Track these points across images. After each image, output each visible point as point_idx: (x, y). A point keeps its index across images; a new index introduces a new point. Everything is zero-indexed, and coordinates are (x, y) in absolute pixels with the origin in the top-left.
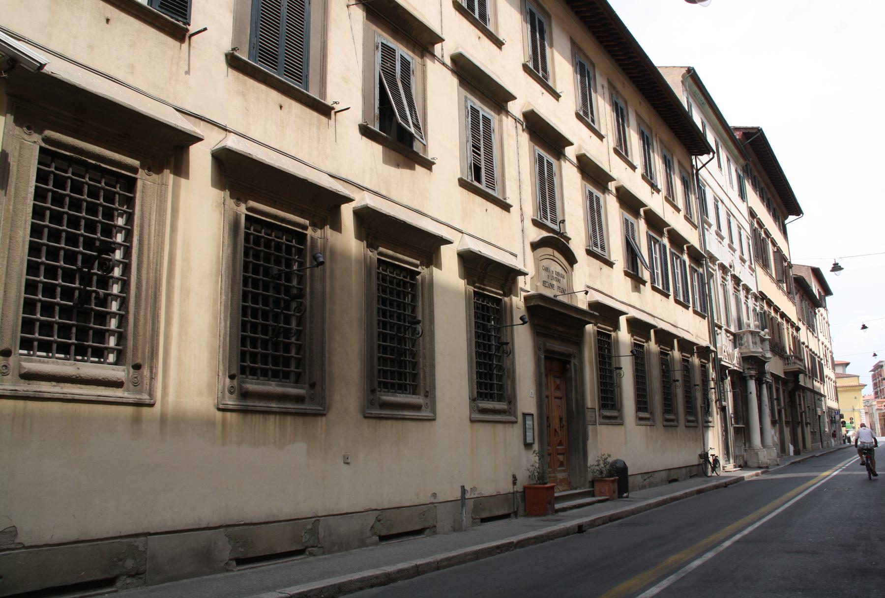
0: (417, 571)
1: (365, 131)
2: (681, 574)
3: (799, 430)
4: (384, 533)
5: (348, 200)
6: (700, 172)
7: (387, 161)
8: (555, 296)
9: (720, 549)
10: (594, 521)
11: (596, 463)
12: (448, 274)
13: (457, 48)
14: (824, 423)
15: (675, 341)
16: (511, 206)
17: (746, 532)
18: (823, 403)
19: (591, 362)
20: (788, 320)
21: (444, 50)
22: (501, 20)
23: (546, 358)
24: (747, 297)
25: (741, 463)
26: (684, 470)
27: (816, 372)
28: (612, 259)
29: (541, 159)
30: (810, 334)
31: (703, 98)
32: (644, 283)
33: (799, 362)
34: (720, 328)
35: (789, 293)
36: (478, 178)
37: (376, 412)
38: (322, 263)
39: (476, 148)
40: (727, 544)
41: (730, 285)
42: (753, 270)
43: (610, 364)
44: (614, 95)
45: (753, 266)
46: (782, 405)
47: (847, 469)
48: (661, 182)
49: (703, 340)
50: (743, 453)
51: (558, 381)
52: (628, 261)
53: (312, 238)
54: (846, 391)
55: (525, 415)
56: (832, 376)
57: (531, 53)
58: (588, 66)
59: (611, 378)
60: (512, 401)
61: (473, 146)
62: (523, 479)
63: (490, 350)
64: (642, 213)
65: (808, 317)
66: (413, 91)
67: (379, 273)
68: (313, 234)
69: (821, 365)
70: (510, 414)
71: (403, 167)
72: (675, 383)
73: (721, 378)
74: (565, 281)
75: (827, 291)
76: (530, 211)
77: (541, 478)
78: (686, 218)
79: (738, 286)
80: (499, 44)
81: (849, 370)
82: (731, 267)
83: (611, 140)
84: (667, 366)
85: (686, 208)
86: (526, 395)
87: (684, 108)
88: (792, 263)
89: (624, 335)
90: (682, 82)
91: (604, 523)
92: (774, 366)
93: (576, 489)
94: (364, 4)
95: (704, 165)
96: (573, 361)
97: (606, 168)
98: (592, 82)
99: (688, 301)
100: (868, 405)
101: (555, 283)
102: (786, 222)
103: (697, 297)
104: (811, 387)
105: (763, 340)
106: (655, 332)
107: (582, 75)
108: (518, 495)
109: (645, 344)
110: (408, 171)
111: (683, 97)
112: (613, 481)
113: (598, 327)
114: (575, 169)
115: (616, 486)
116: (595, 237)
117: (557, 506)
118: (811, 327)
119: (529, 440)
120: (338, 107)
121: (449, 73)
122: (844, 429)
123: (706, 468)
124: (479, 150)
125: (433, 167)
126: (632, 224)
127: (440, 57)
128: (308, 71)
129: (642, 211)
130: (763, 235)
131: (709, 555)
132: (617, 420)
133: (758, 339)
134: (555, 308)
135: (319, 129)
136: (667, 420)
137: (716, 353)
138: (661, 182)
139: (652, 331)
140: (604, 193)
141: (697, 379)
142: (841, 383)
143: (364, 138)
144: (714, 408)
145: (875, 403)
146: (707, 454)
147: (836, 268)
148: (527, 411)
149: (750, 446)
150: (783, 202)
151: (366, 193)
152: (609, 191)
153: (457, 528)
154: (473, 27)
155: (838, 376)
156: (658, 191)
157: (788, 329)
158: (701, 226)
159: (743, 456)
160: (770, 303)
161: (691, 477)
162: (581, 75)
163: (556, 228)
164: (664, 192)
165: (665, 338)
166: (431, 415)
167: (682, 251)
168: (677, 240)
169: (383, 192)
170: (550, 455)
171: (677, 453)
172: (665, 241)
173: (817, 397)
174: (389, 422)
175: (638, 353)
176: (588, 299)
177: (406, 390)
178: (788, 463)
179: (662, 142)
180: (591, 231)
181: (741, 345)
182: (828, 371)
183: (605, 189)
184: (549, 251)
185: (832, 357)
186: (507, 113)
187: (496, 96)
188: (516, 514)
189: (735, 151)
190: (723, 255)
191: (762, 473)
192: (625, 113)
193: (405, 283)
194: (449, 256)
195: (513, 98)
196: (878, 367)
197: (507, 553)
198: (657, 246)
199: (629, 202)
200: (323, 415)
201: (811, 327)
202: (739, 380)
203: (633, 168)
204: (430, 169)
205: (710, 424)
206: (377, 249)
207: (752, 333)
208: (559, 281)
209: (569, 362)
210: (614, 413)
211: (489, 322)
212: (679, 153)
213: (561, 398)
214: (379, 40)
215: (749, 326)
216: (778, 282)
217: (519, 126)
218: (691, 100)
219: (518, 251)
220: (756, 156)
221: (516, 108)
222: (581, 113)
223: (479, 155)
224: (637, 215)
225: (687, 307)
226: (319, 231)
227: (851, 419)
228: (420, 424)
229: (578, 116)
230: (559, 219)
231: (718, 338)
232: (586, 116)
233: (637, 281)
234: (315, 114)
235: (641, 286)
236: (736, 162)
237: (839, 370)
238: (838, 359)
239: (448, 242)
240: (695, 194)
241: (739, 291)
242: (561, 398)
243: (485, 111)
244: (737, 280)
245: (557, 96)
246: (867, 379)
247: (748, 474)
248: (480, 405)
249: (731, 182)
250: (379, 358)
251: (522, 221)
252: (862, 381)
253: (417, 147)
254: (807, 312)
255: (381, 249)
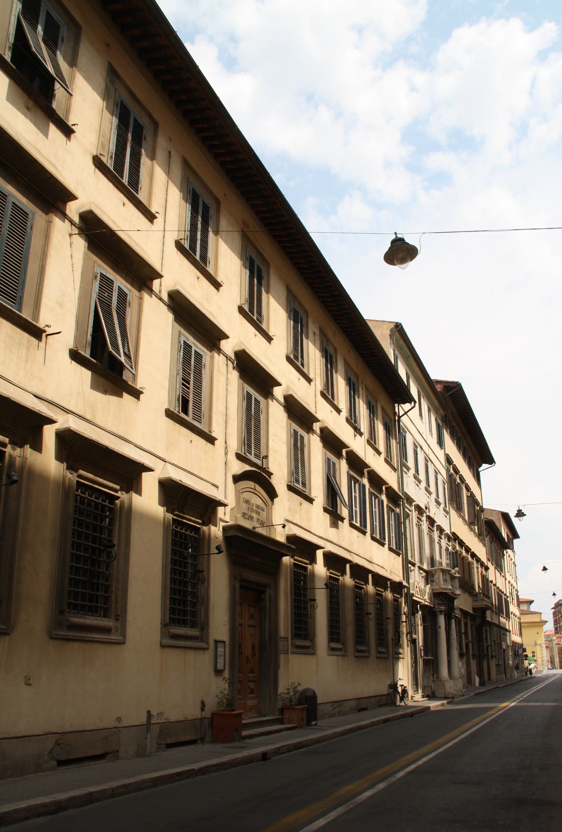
0: (90, 798)
1: (75, 356)
2: (350, 805)
3: (485, 662)
4: (64, 757)
5: (51, 421)
6: (402, 419)
7: (95, 386)
8: (254, 528)
9: (393, 779)
10: (279, 748)
11: (286, 691)
12: (147, 500)
13: (175, 285)
14: (508, 656)
15: (370, 576)
16: (216, 439)
17: (420, 763)
18: (508, 638)
19: (286, 593)
20: (478, 560)
21: (162, 286)
22: (221, 263)
23: (241, 587)
24: (440, 537)
25: (429, 693)
26: (373, 699)
27: (502, 608)
28: (312, 496)
29: (249, 397)
30: (498, 574)
31: (408, 352)
32: (342, 519)
33: (486, 599)
34: (414, 565)
35: (480, 535)
36: (185, 410)
37: (62, 633)
38: (16, 481)
39: (185, 381)
40: (401, 774)
41: (425, 525)
42: (447, 513)
43: (305, 596)
44: (325, 343)
45: (447, 509)
46: (470, 638)
47: (524, 700)
48: (364, 426)
49: (397, 576)
50: (431, 683)
51: (252, 610)
52: (328, 497)
53: (10, 456)
54: (530, 627)
55: (216, 642)
56: (517, 612)
57: (247, 296)
58: (301, 314)
59: (306, 609)
60: (204, 627)
61: (183, 379)
62: (212, 704)
63: (185, 576)
64: (344, 453)
65: (496, 557)
66: (128, 322)
67: (77, 495)
68: (12, 452)
69: (507, 603)
70: (202, 641)
71: (110, 394)
72: (366, 616)
73: (413, 612)
74: (265, 513)
75: (515, 534)
76: (234, 445)
77: (230, 704)
78: (386, 461)
79: (433, 526)
80: (217, 285)
81: (533, 608)
82: (426, 508)
83: (319, 383)
84: (361, 599)
85: (387, 452)
86: (219, 622)
87: (391, 362)
88: (484, 507)
89: (320, 568)
90: (390, 335)
91: (289, 751)
92: (463, 602)
93: (265, 716)
94: (86, 235)
95: (406, 413)
96: (268, 591)
97: (312, 409)
98: (304, 329)
99: (384, 539)
100: (549, 640)
101: (254, 515)
102: (480, 469)
103: (393, 535)
104: (497, 622)
105: (453, 578)
106: (351, 567)
107: (296, 321)
108: (206, 721)
109: (341, 578)
110: (116, 398)
111: (390, 352)
112: (302, 710)
113: (295, 560)
114: (282, 409)
115: (304, 714)
116: (297, 473)
117: (244, 733)
118: (499, 567)
119: (220, 666)
120: (49, 331)
121: (165, 308)
122: (526, 663)
123: (395, 697)
124: (189, 384)
125: (141, 396)
126: (334, 464)
127: (158, 292)
128: (23, 293)
129: (344, 452)
130: (458, 481)
131: (381, 786)
132: (309, 649)
133: (448, 577)
134: (253, 540)
135: (28, 349)
136: (358, 651)
137: (408, 589)
138: (364, 426)
139: (348, 566)
140: (308, 433)
141: (390, 613)
142: (526, 619)
143: (73, 362)
144: (405, 641)
145: (554, 638)
146: (396, 684)
147: (520, 514)
148: (219, 638)
149: (438, 677)
150: (478, 453)
151: (70, 416)
152: (313, 432)
153: (141, 753)
154: (193, 268)
155: (523, 613)
156: (361, 434)
157: (477, 568)
158: (401, 468)
159: (431, 687)
160: (462, 544)
161: (380, 706)
162: (294, 321)
163: (259, 462)
164: (366, 435)
165: (360, 572)
166: (121, 638)
167: (380, 492)
168: (377, 481)
169: (88, 417)
170: (240, 682)
171: (369, 684)
172: (365, 481)
173: (502, 632)
174: (76, 644)
175: (332, 586)
176: (286, 533)
177: (96, 612)
178: (472, 694)
179: (367, 389)
180: (293, 468)
181: (433, 581)
182: (513, 608)
183: (309, 430)
184: (251, 484)
185: (517, 596)
186: (219, 351)
187: (210, 335)
188: (202, 740)
189: (436, 403)
190: (419, 496)
191: (448, 703)
192: (334, 360)
193: (103, 506)
194: (150, 483)
195: (226, 337)
196: (559, 605)
197: (188, 780)
198: (357, 485)
199: (332, 442)
200: (7, 634)
201: (499, 567)
202: (430, 614)
203: (339, 411)
204: (138, 398)
205: (400, 656)
206: (76, 471)
207: (444, 571)
208: (258, 513)
209: (264, 592)
210: (307, 643)
211: (187, 549)
212: (382, 400)
213: (254, 627)
214: (98, 270)
215: (441, 564)
216: (470, 524)
217: (230, 364)
218: (397, 352)
219: (220, 482)
220: (454, 410)
221: (228, 346)
222: (292, 357)
223: (188, 388)
224: (339, 455)
225: (383, 545)
226: (19, 449)
227: (533, 652)
228: (108, 647)
229: (288, 359)
230: (263, 453)
231: (412, 574)
232: (296, 359)
233: (336, 519)
234: (26, 335)
235: (340, 522)
236: (437, 412)
237: (524, 607)
238: (523, 596)
239: (150, 470)
240: (396, 439)
241: (433, 531)
242: (254, 627)
243: (197, 346)
244: (431, 521)
245: (269, 339)
246: (548, 616)
247: (434, 705)
248: (172, 631)
249: (431, 430)
250: (71, 579)
251: (226, 454)
252: (544, 618)
253: (126, 376)
254: (496, 553)
255: (81, 472)
